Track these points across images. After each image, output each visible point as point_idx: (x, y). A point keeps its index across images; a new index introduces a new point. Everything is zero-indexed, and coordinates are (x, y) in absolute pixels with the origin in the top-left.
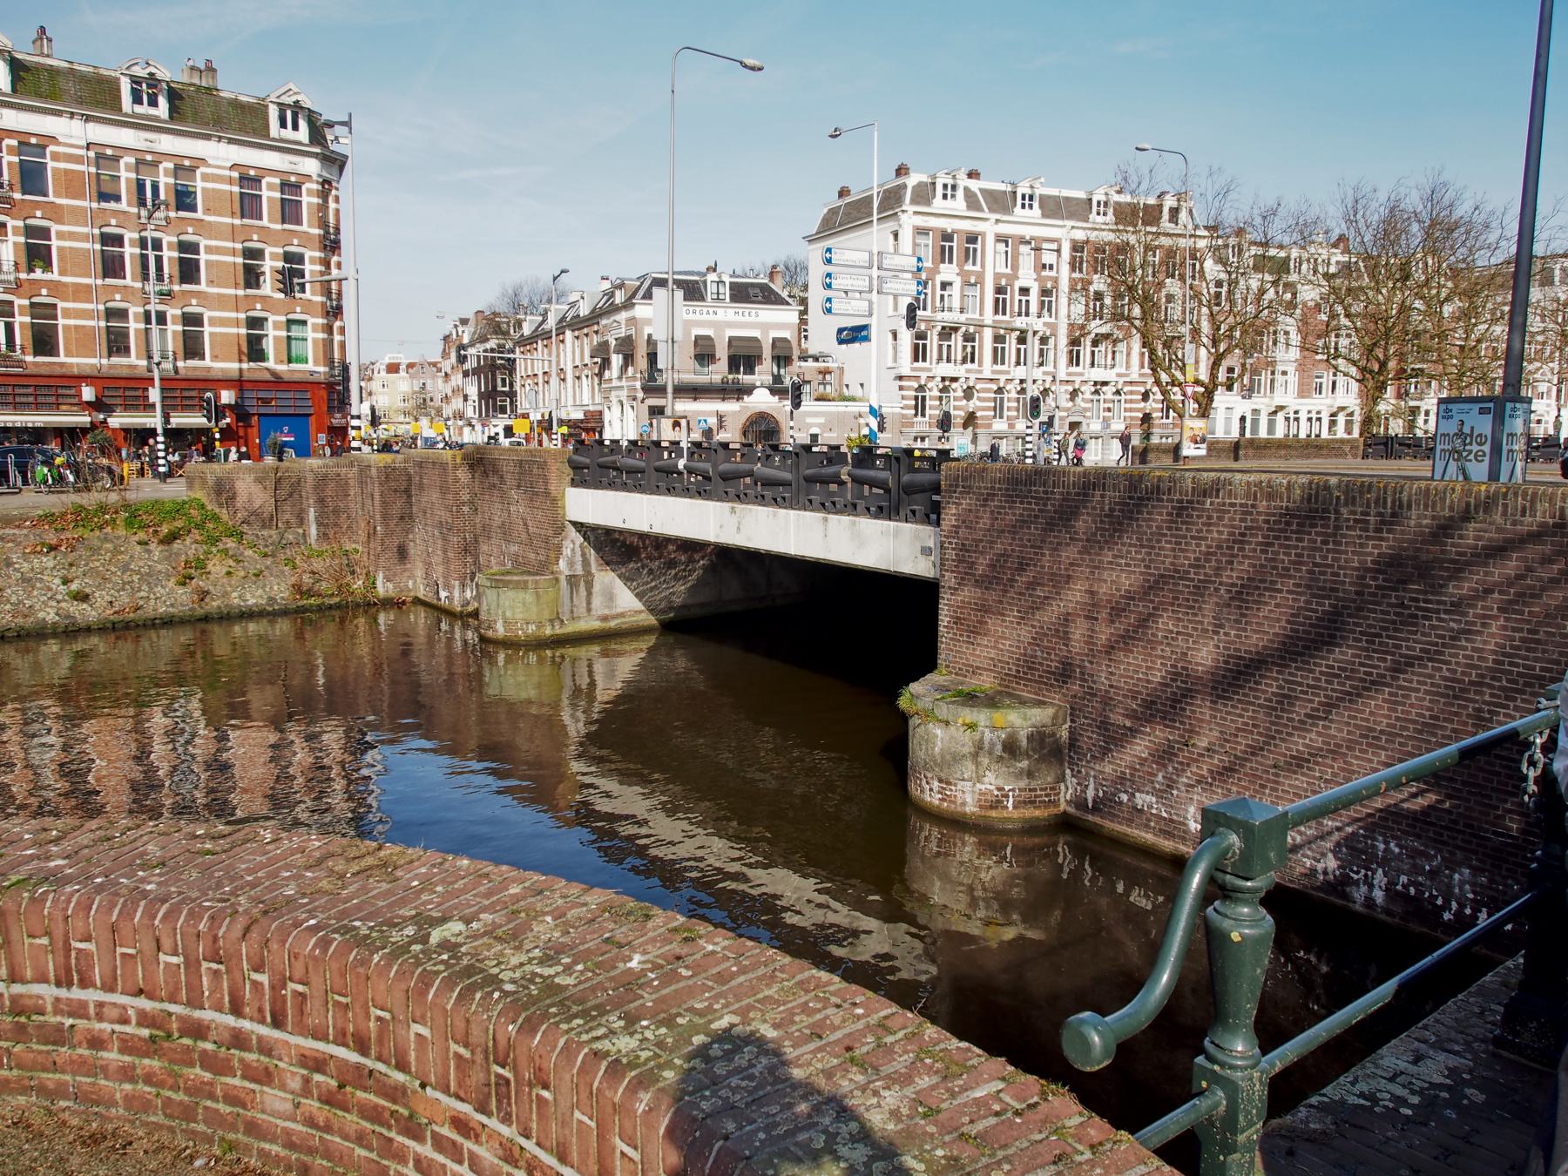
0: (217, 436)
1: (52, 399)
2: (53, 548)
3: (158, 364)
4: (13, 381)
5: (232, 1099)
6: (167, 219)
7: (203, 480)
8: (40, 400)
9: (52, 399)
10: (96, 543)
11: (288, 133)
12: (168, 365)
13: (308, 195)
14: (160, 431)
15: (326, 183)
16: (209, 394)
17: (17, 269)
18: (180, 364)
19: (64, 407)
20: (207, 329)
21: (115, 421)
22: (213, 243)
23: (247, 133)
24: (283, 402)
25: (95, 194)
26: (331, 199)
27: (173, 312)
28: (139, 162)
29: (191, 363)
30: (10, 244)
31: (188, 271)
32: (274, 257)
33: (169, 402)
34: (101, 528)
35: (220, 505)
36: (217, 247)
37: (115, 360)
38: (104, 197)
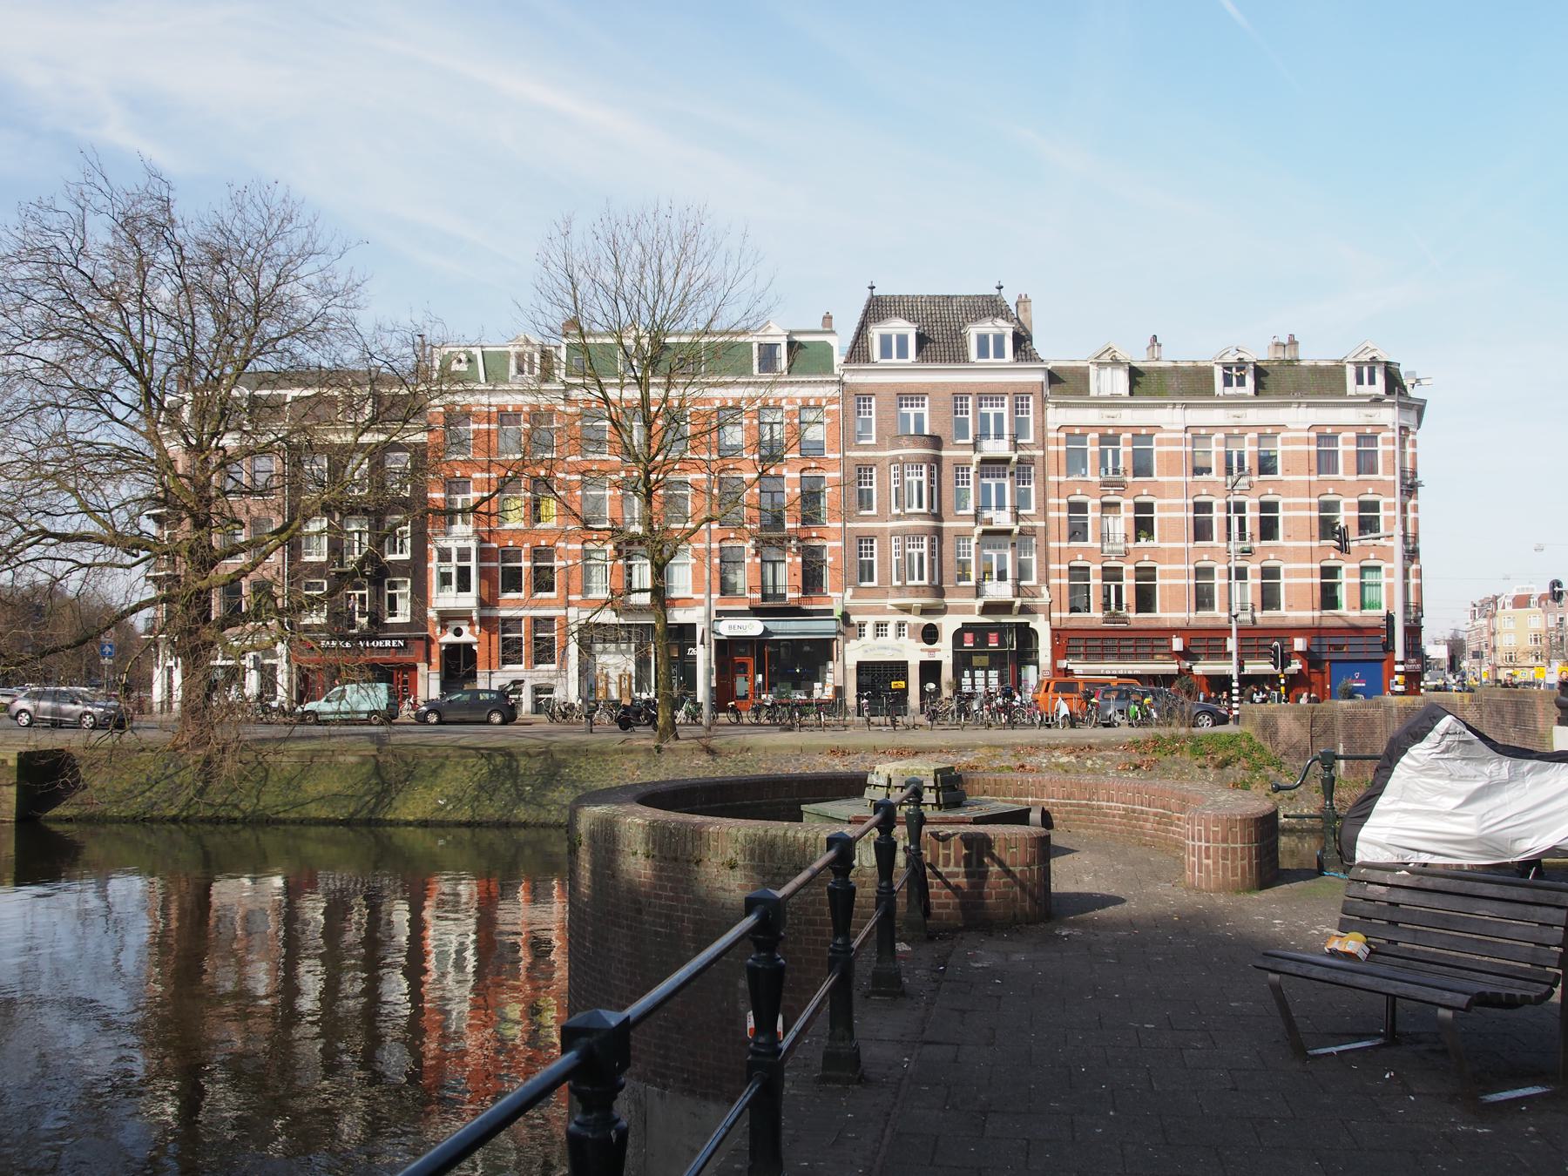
0: (1283, 681)
1: (1148, 650)
2: (1137, 767)
3: (1236, 616)
4: (1118, 635)
5: (1141, 827)
6: (1251, 484)
7: (1253, 718)
8: (1140, 650)
9: (1148, 650)
10: (1168, 765)
11: (1365, 388)
12: (1246, 617)
13: (1384, 444)
14: (1235, 677)
15: (1404, 429)
16: (1276, 643)
17: (1126, 540)
18: (1258, 614)
19: (1158, 657)
20: (1283, 581)
21: (1198, 669)
22: (1291, 500)
23: (1324, 395)
24: (1354, 648)
25: (1190, 470)
26: (1407, 444)
27: (1253, 567)
28: (1228, 436)
29: (1267, 613)
30: (1122, 519)
31: (1268, 529)
32: (1348, 507)
33: (1246, 650)
34: (1172, 753)
35: (1265, 739)
36: (1294, 504)
37: (1201, 613)
38: (1198, 471)
